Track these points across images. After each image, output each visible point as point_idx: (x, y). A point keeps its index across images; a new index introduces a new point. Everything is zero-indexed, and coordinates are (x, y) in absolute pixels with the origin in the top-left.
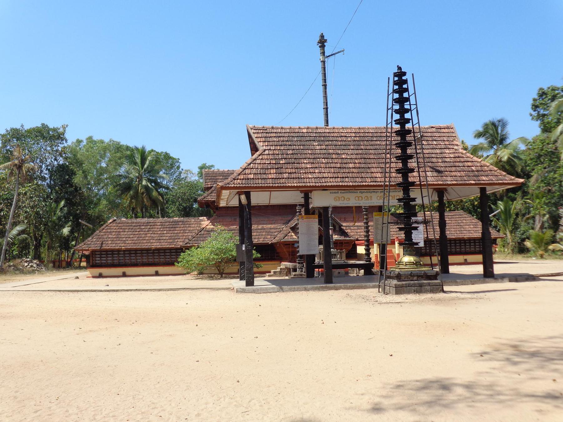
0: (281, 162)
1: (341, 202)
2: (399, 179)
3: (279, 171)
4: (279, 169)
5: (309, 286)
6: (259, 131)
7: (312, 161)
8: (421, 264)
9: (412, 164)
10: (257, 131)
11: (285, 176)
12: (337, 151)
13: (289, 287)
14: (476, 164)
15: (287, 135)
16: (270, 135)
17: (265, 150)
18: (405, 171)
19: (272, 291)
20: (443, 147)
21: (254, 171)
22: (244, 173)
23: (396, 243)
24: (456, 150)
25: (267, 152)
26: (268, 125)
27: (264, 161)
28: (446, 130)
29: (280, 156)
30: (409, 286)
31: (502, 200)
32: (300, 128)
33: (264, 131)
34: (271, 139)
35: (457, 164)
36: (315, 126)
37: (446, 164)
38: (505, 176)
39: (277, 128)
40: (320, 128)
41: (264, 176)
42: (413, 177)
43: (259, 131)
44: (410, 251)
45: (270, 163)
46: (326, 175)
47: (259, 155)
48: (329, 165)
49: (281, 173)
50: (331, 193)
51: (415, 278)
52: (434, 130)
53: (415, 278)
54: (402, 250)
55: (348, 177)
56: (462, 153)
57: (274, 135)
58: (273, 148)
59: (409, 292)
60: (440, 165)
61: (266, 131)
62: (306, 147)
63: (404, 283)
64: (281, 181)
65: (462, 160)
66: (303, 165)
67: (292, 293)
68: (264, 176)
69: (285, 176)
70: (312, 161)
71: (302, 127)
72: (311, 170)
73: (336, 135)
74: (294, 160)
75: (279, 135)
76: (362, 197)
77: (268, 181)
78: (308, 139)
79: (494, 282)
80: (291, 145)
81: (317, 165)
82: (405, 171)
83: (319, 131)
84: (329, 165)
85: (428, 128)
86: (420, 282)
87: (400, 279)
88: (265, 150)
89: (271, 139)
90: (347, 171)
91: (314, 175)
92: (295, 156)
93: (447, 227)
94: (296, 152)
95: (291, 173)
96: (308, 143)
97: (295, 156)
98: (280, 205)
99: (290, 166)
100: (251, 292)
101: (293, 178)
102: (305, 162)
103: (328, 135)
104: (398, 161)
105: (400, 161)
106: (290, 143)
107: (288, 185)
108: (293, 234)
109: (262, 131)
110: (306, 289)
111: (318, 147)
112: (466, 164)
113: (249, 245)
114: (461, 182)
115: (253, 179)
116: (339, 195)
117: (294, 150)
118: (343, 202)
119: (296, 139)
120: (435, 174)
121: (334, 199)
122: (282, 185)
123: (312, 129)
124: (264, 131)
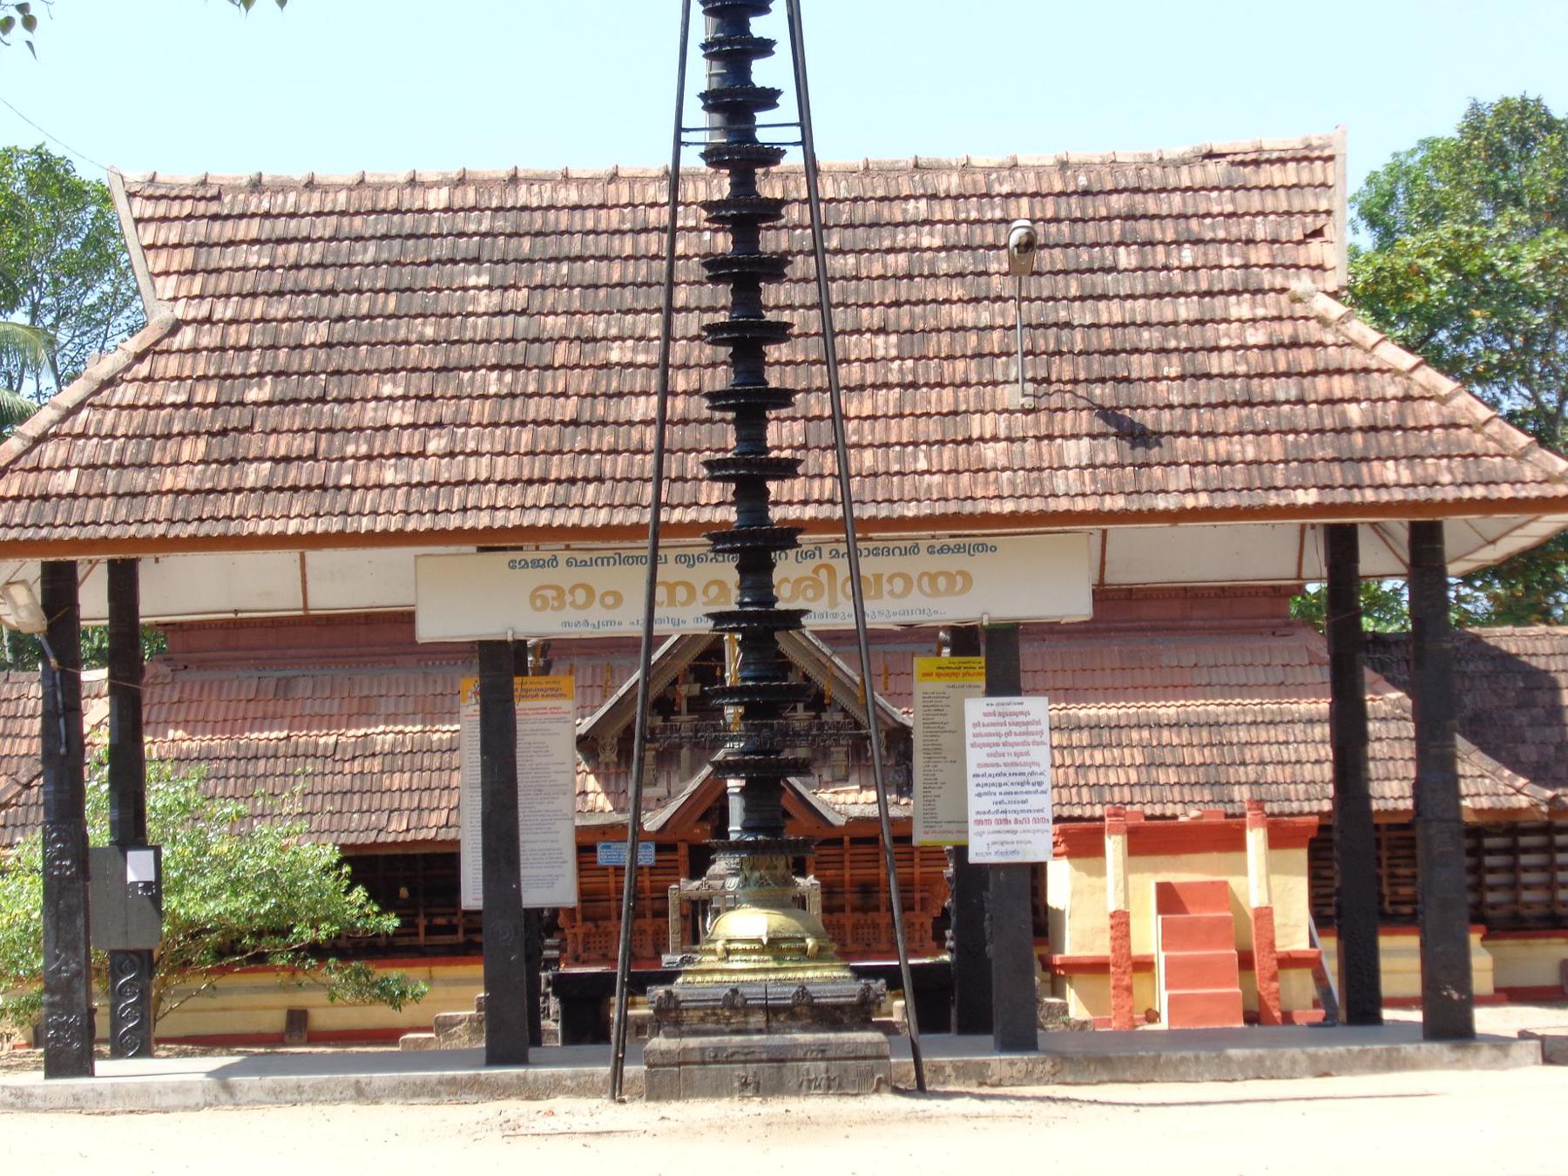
0: (252, 395)
1: (570, 614)
2: (716, 505)
3: (226, 447)
4: (227, 433)
5: (381, 1078)
6: (175, 209)
7: (423, 384)
8: (804, 950)
9: (780, 434)
10: (161, 209)
11: (255, 474)
12: (589, 321)
13: (269, 1080)
14: (1378, 383)
15: (325, 227)
16: (227, 230)
17: (176, 327)
18: (751, 473)
19: (171, 1100)
20: (1225, 280)
21: (89, 450)
22: (29, 461)
23: (1256, 838)
24: (1296, 300)
25: (186, 337)
26: (231, 168)
27: (156, 393)
28: (1290, 174)
29: (255, 356)
30: (719, 1057)
31: (1370, 616)
32: (412, 182)
33: (202, 207)
34: (229, 258)
35: (1267, 387)
36: (502, 170)
37: (1206, 391)
38: (1521, 456)
39: (283, 188)
40: (530, 181)
41: (138, 480)
42: (788, 501)
43: (175, 209)
44: (761, 883)
45: (188, 405)
46: (477, 468)
47: (140, 357)
48: (516, 409)
49: (233, 461)
50: (512, 565)
51: (758, 1019)
52: (1215, 171)
53: (758, 1019)
54: (1299, 887)
55: (600, 479)
56: (1323, 321)
57: (253, 229)
58: (224, 310)
59: (716, 1090)
60: (1163, 394)
61: (214, 208)
62: (417, 301)
63: (693, 1042)
64: (224, 506)
65: (1306, 360)
66: (371, 414)
67: (288, 1110)
68: (138, 480)
69: (255, 474)
70: (423, 384)
71: (428, 173)
72: (409, 442)
73: (613, 219)
74: (320, 388)
75: (280, 227)
76: (690, 588)
77: (153, 508)
78: (442, 248)
79: (1451, 1065)
80: (333, 292)
81: (447, 411)
82: (751, 473)
83: (523, 196)
84: (516, 409)
85: (1179, 163)
86: (776, 1039)
87: (678, 1023)
88: (176, 327)
89: (229, 258)
90: (608, 440)
91: (418, 471)
92: (337, 359)
93: (1374, 749)
94: (349, 330)
95: (287, 459)
96: (432, 276)
97: (337, 359)
98: (367, 615)
99: (291, 417)
100: (63, 1109)
101: (295, 489)
102: (387, 390)
103: (564, 219)
104: (718, 415)
105: (730, 415)
106: (329, 278)
107: (248, 528)
108: (592, 783)
109: (188, 207)
110: (361, 1094)
111: (486, 301)
112: (1321, 385)
113: (62, 855)
114: (1245, 500)
115: (73, 496)
116: (563, 576)
117: (342, 318)
118: (581, 615)
119: (370, 252)
120: (1110, 450)
121: (534, 596)
122: (218, 529)
123: (483, 185)
124: (202, 207)
